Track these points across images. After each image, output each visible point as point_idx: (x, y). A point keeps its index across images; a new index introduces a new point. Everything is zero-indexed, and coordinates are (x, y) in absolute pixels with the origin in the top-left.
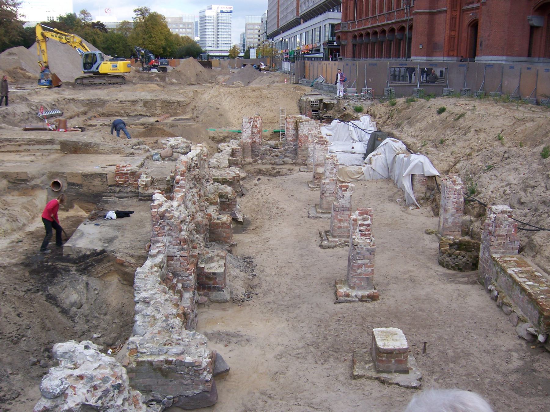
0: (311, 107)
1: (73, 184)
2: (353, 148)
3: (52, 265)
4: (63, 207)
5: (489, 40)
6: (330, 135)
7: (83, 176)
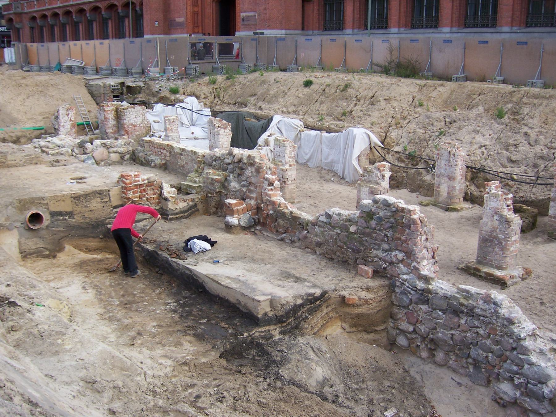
0: (112, 92)
1: (60, 214)
2: (193, 133)
3: (250, 336)
4: (48, 253)
5: (266, 14)
6: (158, 122)
7: (74, 198)
